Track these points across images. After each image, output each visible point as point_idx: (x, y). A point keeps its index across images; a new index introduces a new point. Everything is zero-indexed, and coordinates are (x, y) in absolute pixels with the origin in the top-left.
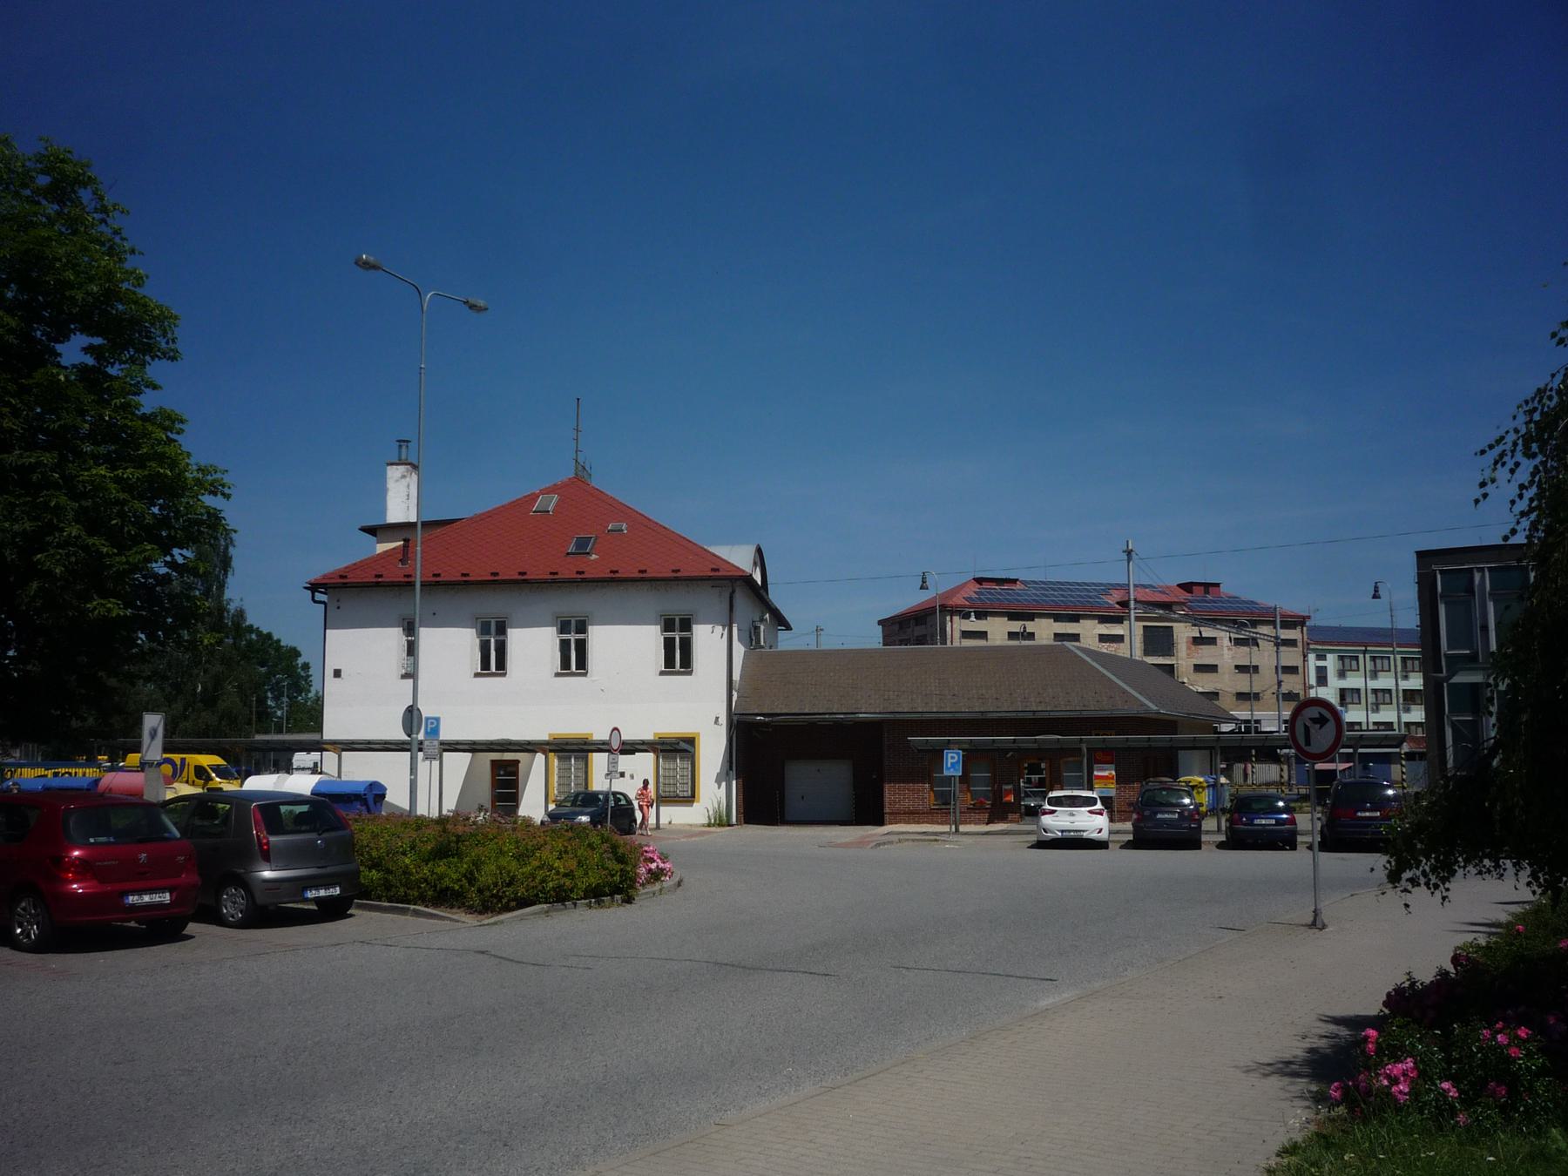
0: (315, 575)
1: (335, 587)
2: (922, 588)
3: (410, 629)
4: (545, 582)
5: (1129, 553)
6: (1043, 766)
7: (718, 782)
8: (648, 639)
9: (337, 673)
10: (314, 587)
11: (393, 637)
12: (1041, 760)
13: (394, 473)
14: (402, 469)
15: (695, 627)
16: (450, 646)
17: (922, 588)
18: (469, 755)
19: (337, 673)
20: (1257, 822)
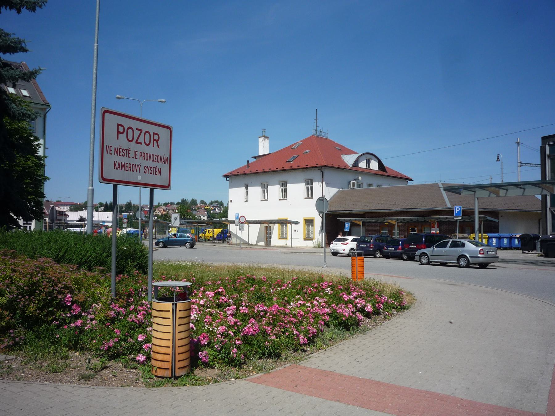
0: (226, 172)
1: (231, 176)
2: (497, 161)
3: (247, 188)
4: (268, 172)
5: (518, 143)
6: (416, 229)
7: (319, 233)
8: (302, 187)
9: (231, 201)
10: (226, 176)
11: (243, 189)
12: (415, 226)
13: (261, 140)
14: (262, 138)
15: (314, 183)
16: (256, 191)
17: (497, 161)
18: (259, 225)
19: (231, 201)
20: (389, 249)
